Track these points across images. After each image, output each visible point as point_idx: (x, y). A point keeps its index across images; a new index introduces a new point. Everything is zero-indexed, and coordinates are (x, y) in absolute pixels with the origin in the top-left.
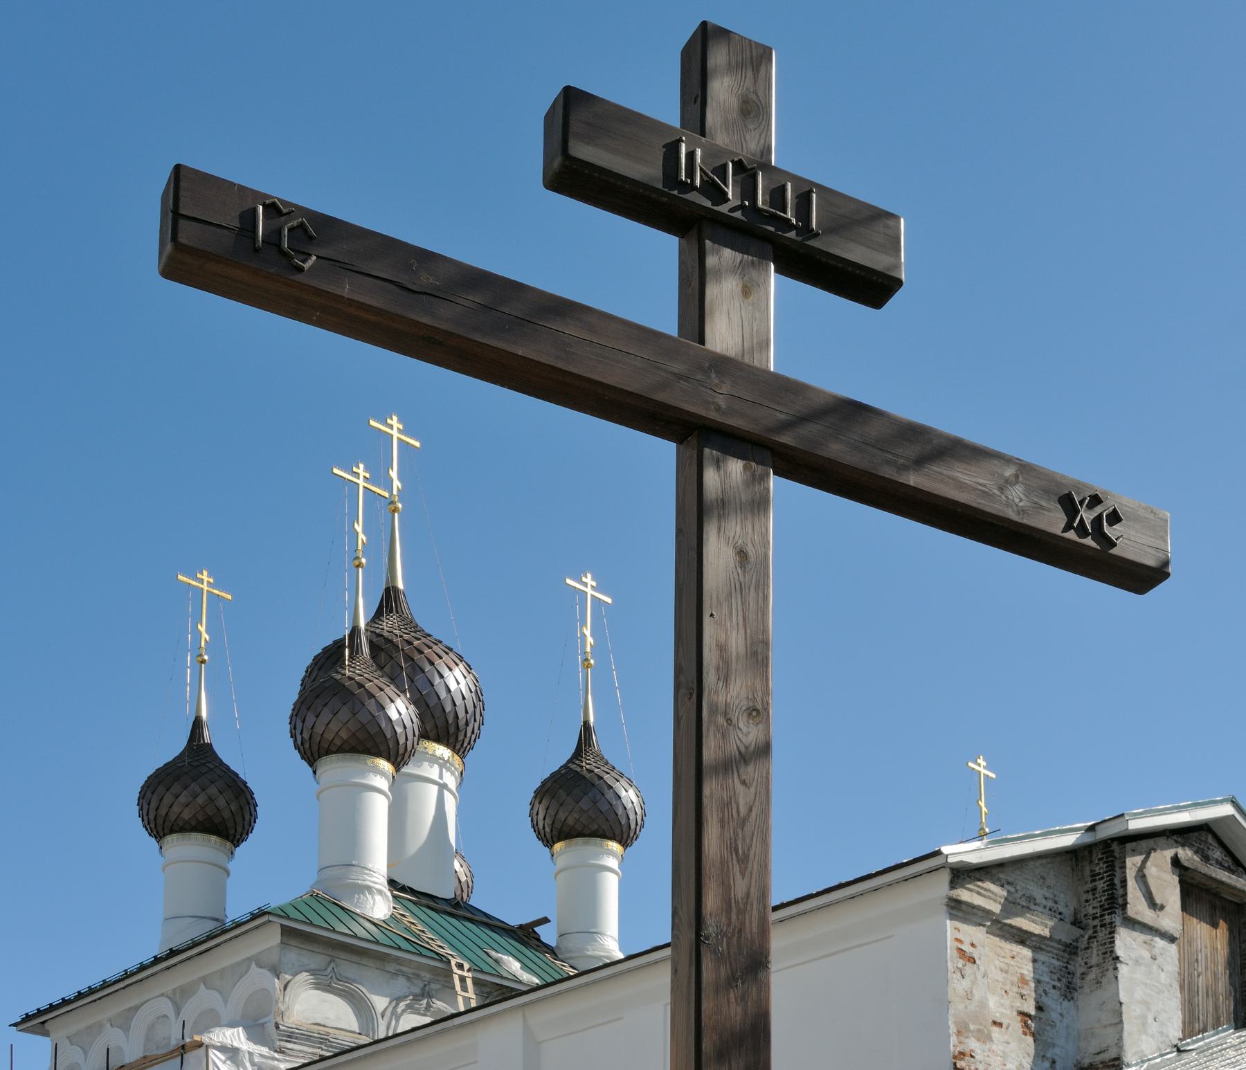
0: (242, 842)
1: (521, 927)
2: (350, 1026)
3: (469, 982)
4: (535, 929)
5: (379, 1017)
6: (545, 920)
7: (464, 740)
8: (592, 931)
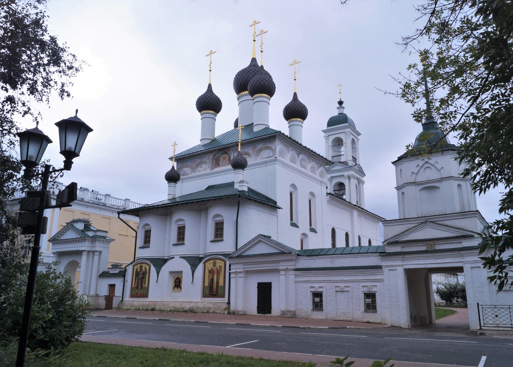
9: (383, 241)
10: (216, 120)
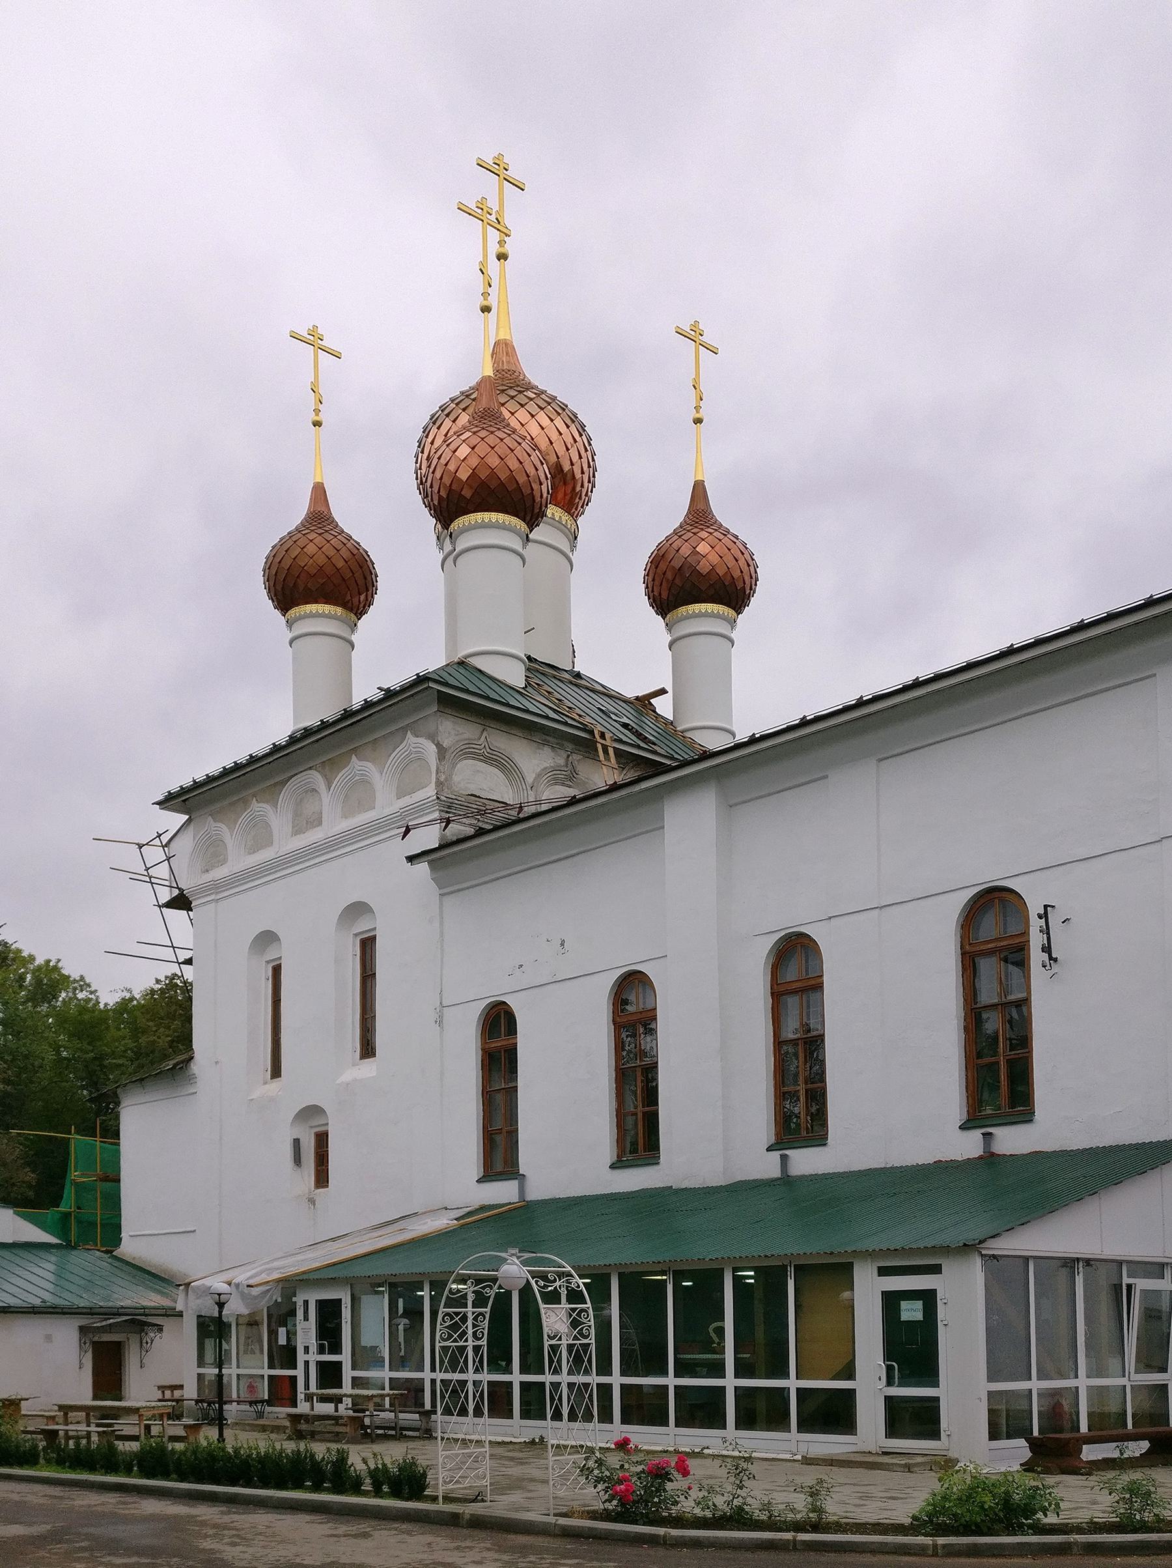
0: (369, 607)
1: (637, 698)
2: (502, 798)
3: (611, 751)
4: (651, 700)
5: (529, 788)
6: (663, 691)
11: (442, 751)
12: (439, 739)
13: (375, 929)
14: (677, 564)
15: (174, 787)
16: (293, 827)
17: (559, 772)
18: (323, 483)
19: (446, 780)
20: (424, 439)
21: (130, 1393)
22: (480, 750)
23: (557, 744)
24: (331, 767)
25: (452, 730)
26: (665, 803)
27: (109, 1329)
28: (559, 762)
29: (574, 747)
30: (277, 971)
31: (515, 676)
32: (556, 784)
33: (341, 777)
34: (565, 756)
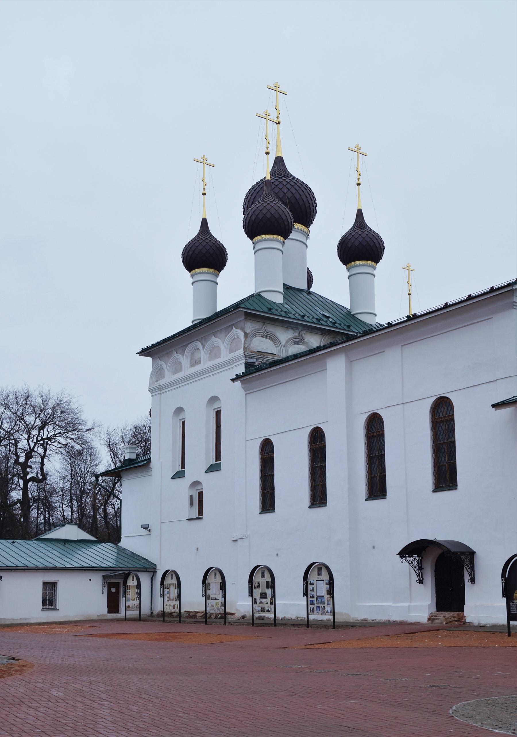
5: (283, 347)
7: (310, 211)
8: (328, 620)
9: (192, 319)
10: (217, 284)
11: (246, 335)
12: (245, 330)
13: (221, 407)
14: (349, 245)
15: (145, 347)
16: (190, 364)
17: (296, 339)
18: (206, 218)
19: (248, 346)
20: (246, 200)
21: (177, 591)
22: (262, 333)
23: (295, 327)
24: (204, 340)
25: (250, 326)
26: (327, 361)
27: (115, 577)
28: (296, 335)
29: (302, 328)
30: (184, 423)
31: (279, 299)
32: (295, 344)
33: (208, 344)
34: (298, 332)
